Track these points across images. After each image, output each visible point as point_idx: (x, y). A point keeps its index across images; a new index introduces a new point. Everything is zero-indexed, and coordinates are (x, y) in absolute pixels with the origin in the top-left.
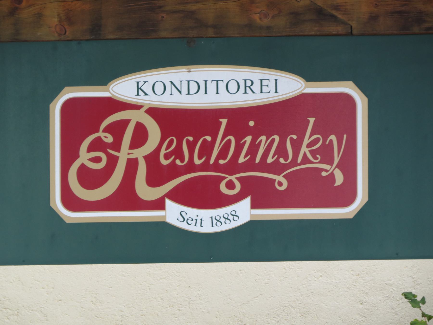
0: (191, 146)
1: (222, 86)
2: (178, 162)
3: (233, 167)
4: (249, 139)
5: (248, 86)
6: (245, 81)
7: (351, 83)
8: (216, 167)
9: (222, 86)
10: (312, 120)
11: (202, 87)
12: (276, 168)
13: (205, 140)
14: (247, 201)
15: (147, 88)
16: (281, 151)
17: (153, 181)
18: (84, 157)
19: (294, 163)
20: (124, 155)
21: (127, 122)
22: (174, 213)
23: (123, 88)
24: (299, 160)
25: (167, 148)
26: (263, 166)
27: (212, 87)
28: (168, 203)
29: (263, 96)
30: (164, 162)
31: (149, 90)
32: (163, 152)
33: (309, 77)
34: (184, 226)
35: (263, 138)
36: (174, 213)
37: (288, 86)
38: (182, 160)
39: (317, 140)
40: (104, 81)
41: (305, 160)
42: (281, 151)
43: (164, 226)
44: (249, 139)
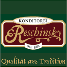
0: (30, 33)
1: (36, 21)
2: (27, 36)
3: (38, 37)
4: (42, 31)
5: (41, 21)
6: (29, 20)
7: (62, 21)
8: (35, 37)
9: (36, 21)
10: (54, 28)
11: (32, 21)
12: (47, 37)
13: (33, 32)
14: (41, 44)
15: (21, 21)
16: (48, 34)
17: (22, 39)
18: (8, 34)
19: (51, 36)
20: (16, 34)
21: (17, 27)
22: (26, 46)
23: (16, 21)
24: (52, 36)
25: (25, 33)
26: (45, 37)
27: (34, 21)
28: (25, 44)
29: (22, 23)
30: (24, 35)
31: (22, 21)
32: (24, 33)
33: (54, 19)
34: (28, 48)
35: (45, 31)
36: (26, 46)
37: (50, 21)
38: (28, 35)
39: (55, 32)
40: (12, 19)
41: (53, 36)
42: (48, 34)
43: (24, 48)
44: (42, 31)
